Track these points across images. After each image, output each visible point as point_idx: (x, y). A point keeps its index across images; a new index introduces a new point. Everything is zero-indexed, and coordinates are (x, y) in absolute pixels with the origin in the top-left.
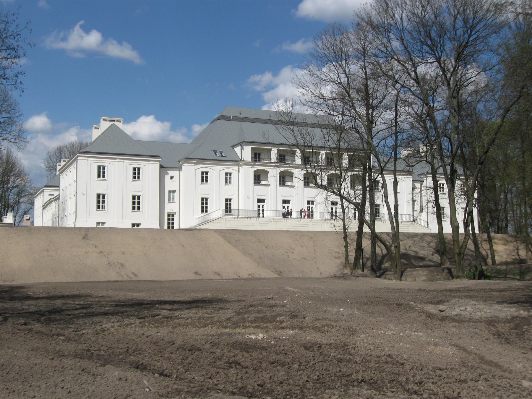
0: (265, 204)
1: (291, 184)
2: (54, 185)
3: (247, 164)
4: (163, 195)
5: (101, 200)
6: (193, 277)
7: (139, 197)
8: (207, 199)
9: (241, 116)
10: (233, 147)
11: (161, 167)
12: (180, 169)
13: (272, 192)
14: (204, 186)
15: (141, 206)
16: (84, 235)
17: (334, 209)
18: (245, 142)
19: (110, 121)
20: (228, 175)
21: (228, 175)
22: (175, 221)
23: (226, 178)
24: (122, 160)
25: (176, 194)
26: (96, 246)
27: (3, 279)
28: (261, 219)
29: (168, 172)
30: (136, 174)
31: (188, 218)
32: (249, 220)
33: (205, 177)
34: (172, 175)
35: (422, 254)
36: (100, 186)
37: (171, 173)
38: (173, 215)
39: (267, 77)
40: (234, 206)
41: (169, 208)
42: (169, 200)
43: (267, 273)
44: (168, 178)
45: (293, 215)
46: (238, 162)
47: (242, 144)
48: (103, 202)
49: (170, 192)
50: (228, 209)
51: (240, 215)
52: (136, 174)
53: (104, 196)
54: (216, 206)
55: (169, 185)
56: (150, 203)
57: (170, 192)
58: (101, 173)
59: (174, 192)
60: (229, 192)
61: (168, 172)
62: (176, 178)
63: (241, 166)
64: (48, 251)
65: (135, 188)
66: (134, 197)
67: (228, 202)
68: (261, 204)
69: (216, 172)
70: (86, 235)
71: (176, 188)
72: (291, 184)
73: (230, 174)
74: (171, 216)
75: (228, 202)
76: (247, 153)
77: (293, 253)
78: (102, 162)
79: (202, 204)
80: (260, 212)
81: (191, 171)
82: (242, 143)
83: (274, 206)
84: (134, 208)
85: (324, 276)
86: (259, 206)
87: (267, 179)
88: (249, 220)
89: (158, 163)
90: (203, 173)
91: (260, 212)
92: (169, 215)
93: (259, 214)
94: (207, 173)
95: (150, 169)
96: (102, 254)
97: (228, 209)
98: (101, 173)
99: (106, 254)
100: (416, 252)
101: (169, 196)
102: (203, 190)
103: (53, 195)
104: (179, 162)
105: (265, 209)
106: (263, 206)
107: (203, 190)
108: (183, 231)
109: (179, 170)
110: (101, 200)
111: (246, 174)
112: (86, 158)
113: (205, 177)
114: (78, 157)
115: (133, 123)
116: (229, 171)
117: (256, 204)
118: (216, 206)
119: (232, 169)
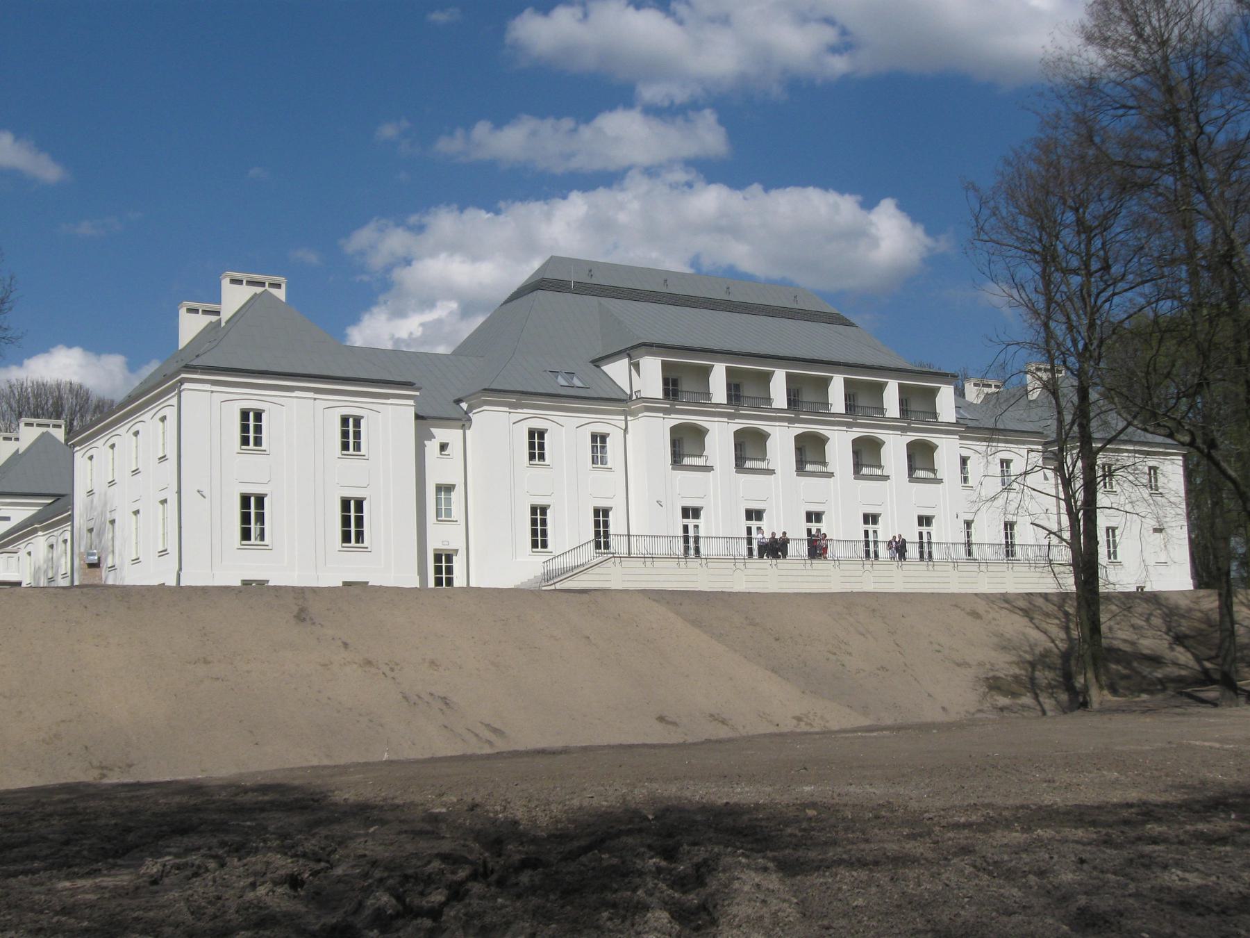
0: (701, 522)
1: (763, 465)
2: (7, 490)
3: (650, 406)
4: (433, 499)
5: (252, 510)
6: (657, 734)
7: (359, 504)
8: (544, 510)
9: (594, 281)
10: (597, 362)
11: (418, 417)
12: (464, 422)
13: (721, 490)
14: (536, 472)
15: (366, 529)
16: (296, 609)
17: (871, 534)
18: (644, 344)
19: (250, 283)
20: (599, 440)
21: (599, 440)
22: (455, 576)
23: (594, 448)
24: (311, 395)
25: (457, 496)
26: (346, 645)
27: (95, 763)
28: (694, 564)
29: (433, 430)
30: (350, 434)
31: (497, 561)
32: (648, 564)
33: (536, 444)
34: (445, 441)
35: (1147, 648)
36: (249, 472)
37: (441, 434)
38: (449, 558)
39: (396, 241)
40: (616, 525)
41: (440, 536)
42: (438, 514)
43: (837, 717)
44: (432, 447)
45: (791, 548)
46: (621, 402)
47: (633, 353)
48: (260, 518)
49: (439, 488)
50: (602, 539)
51: (634, 551)
52: (350, 434)
53: (260, 500)
54: (570, 531)
55: (440, 470)
56: (389, 522)
57: (439, 488)
58: (251, 428)
59: (449, 488)
60: (603, 487)
61: (433, 430)
62: (455, 449)
63: (634, 413)
64: (206, 662)
65: (349, 477)
66: (345, 504)
67: (601, 515)
68: (691, 522)
69: (568, 431)
70: (302, 610)
71: (457, 480)
72: (763, 465)
73: (603, 438)
74: (444, 560)
75: (601, 515)
76: (649, 377)
77: (850, 654)
78: (253, 399)
79: (534, 522)
80: (691, 545)
81: (497, 429)
82: (632, 352)
83: (722, 525)
84: (346, 538)
85: (952, 717)
86: (686, 528)
87: (700, 450)
88: (648, 564)
89: (412, 402)
90: (531, 433)
91: (691, 545)
92: (438, 558)
93: (687, 549)
94: (542, 434)
95: (389, 420)
96: (373, 670)
97: (602, 539)
98: (251, 428)
99: (386, 669)
100: (1133, 643)
101: (438, 500)
102: (534, 484)
103: (8, 519)
104: (458, 401)
105: (701, 534)
106: (696, 527)
107: (534, 484)
108: (567, 595)
109: (463, 427)
110: (252, 510)
111: (649, 434)
112: (208, 387)
113: (536, 444)
114: (182, 382)
115: (756, 188)
116: (600, 429)
117: (680, 521)
118: (570, 531)
119: (610, 424)
